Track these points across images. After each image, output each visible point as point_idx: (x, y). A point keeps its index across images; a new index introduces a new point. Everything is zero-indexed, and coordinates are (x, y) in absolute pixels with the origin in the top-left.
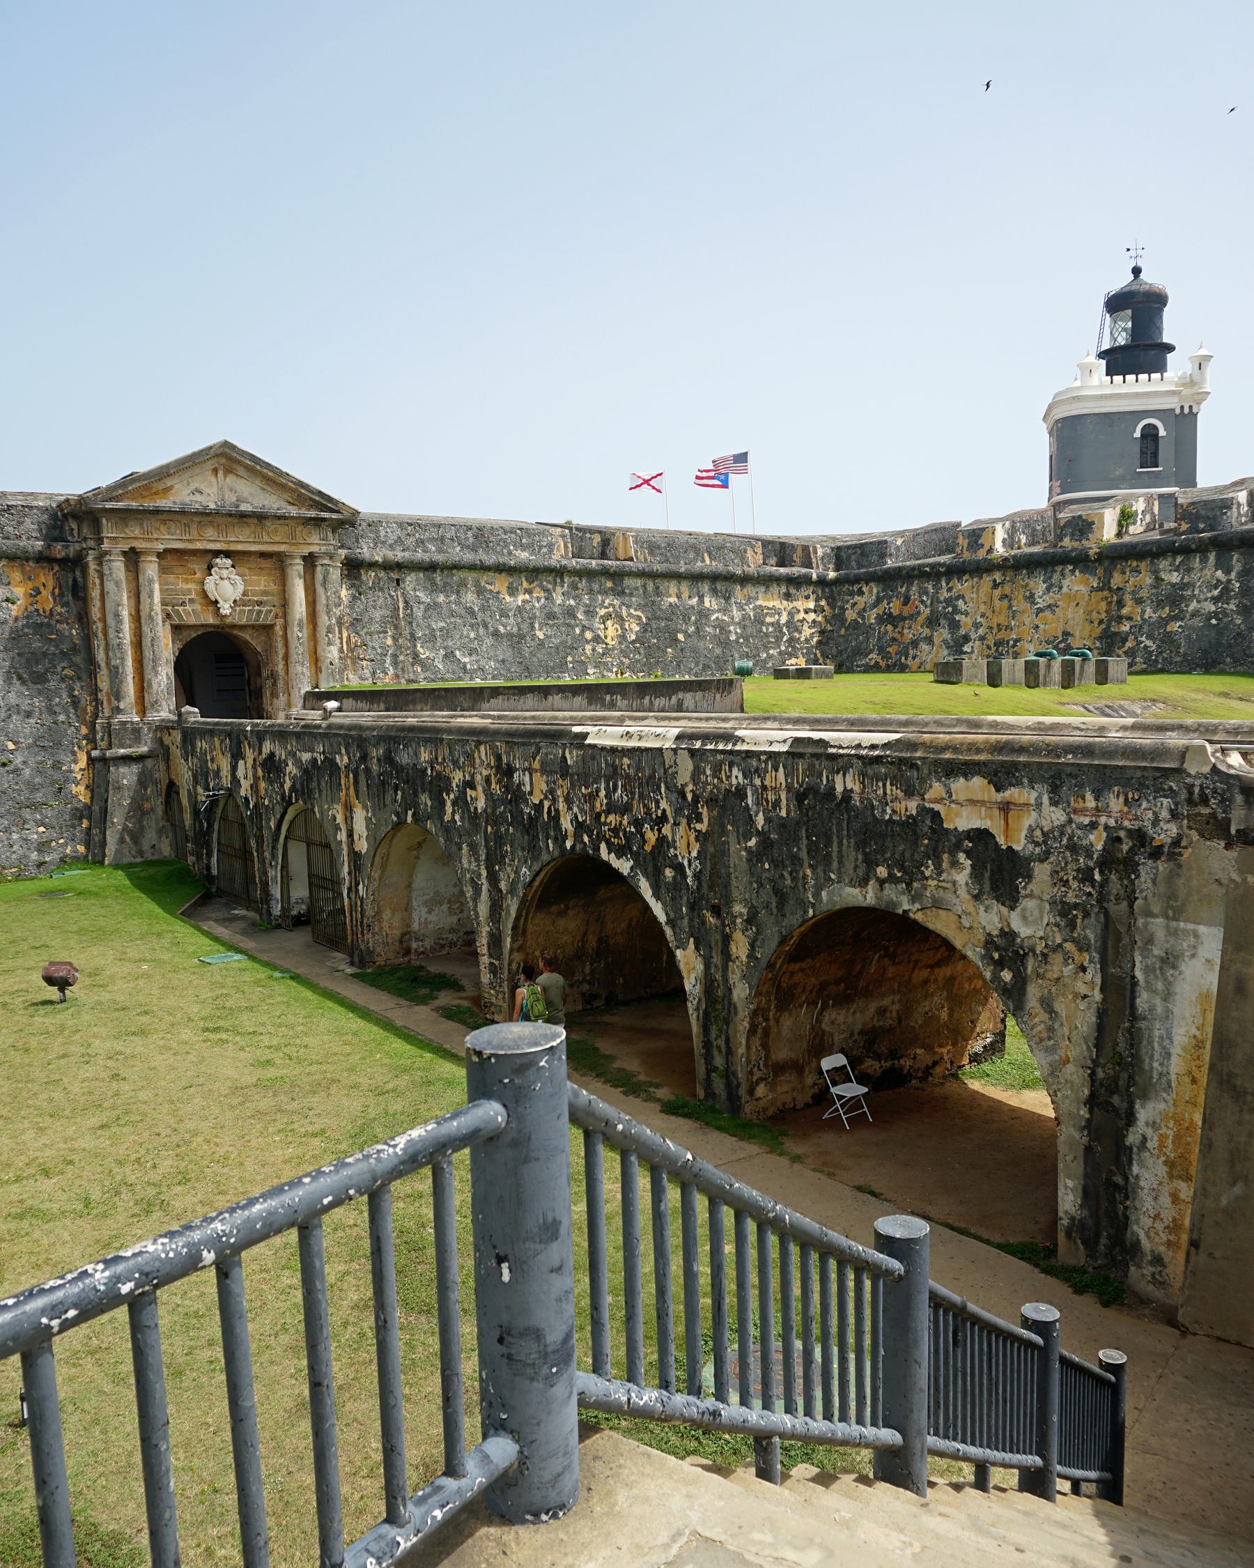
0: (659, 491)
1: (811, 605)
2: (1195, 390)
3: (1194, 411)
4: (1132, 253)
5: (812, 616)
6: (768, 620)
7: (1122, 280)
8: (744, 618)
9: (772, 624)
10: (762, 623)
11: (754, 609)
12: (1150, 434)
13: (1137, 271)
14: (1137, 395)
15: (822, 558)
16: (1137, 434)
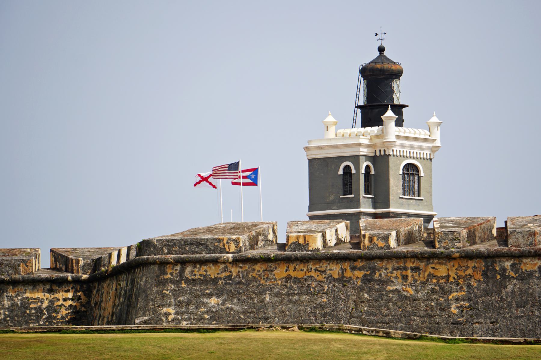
0: (214, 187)
1: (70, 295)
4: (379, 37)
5: (70, 302)
6: (32, 306)
8: (12, 305)
9: (35, 308)
10: (27, 308)
11: (21, 300)
13: (381, 50)
15: (83, 266)
16: (341, 172)
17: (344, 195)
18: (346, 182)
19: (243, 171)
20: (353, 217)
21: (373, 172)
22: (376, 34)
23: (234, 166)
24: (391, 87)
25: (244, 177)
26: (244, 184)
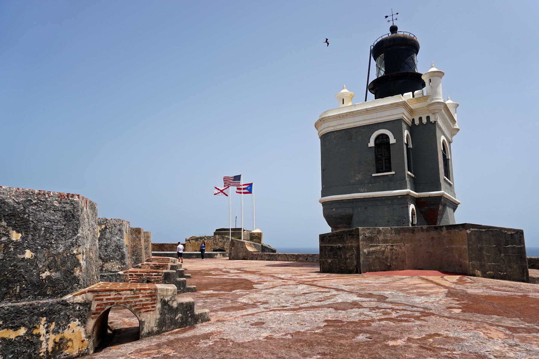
0: (227, 195)
2: (429, 102)
3: (432, 120)
4: (390, 18)
7: (386, 33)
12: (382, 140)
14: (367, 111)
16: (372, 144)
17: (377, 173)
18: (379, 156)
19: (243, 185)
20: (395, 201)
21: (411, 146)
22: (387, 17)
23: (237, 178)
24: (413, 60)
25: (244, 189)
26: (244, 193)
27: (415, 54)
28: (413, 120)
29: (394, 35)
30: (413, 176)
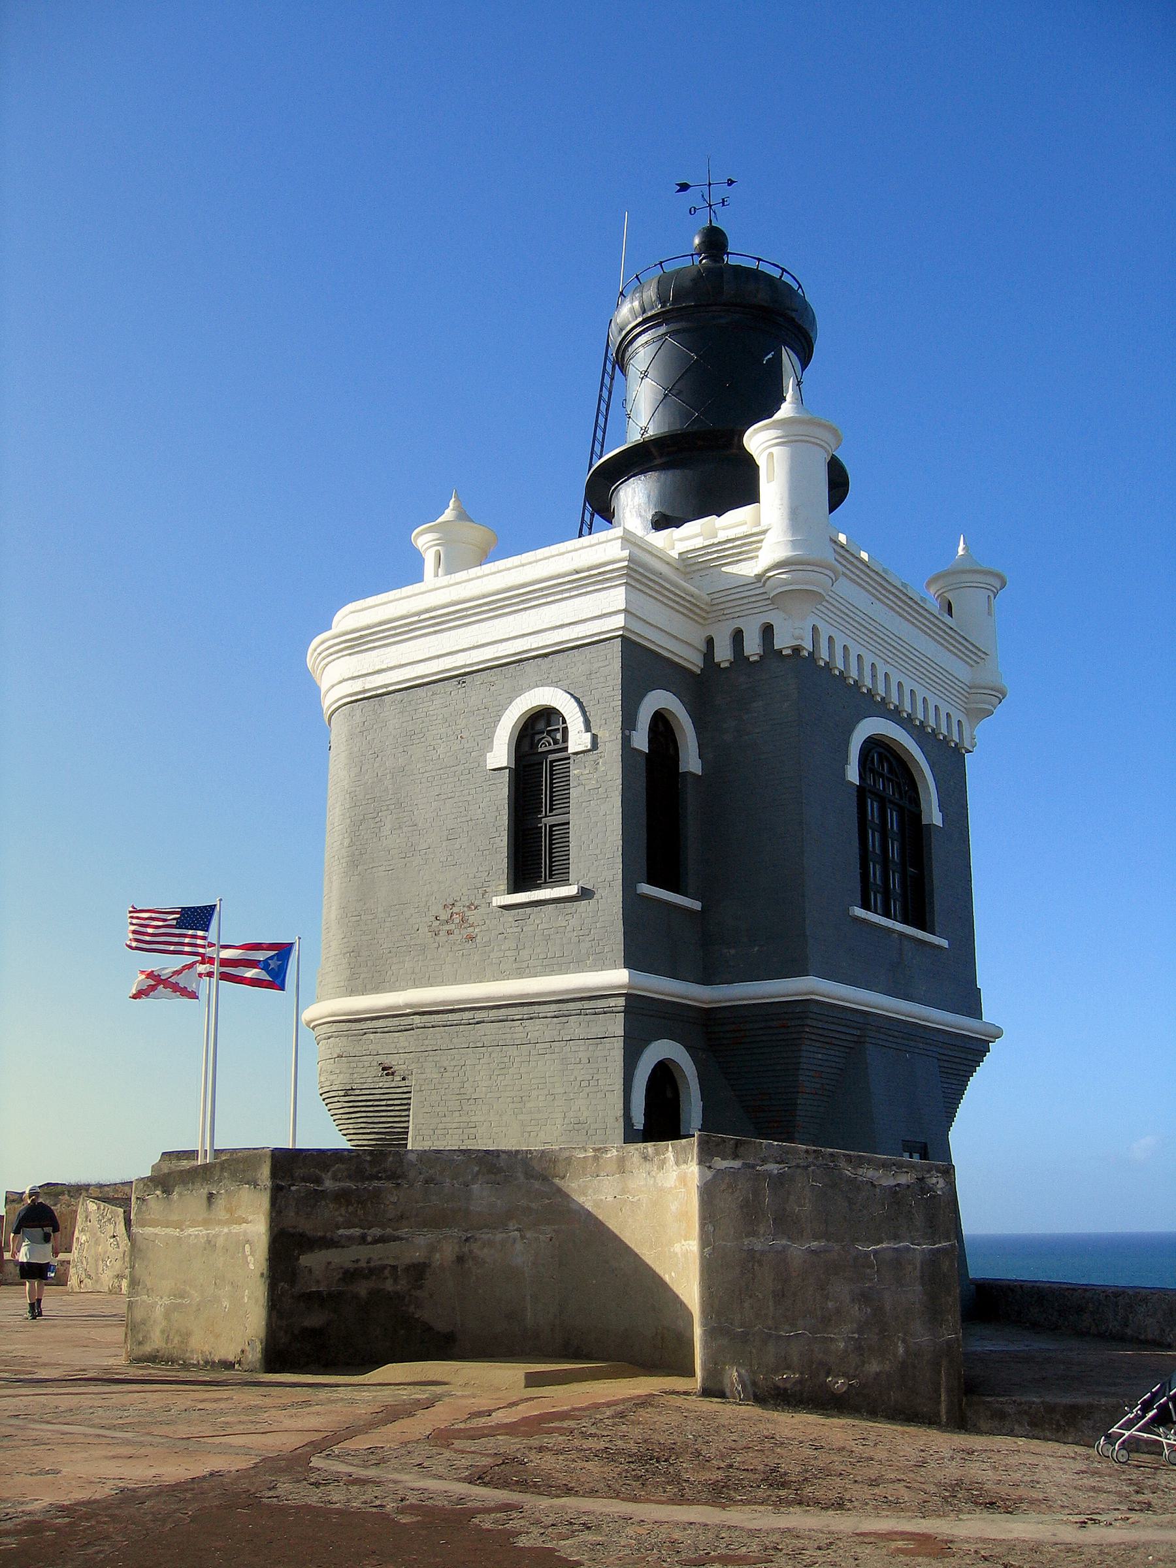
12: (539, 727)
16: (853, 774)
22: (684, 187)
23: (198, 918)
27: (788, 359)
28: (710, 642)
29: (718, 265)
30: (696, 905)
